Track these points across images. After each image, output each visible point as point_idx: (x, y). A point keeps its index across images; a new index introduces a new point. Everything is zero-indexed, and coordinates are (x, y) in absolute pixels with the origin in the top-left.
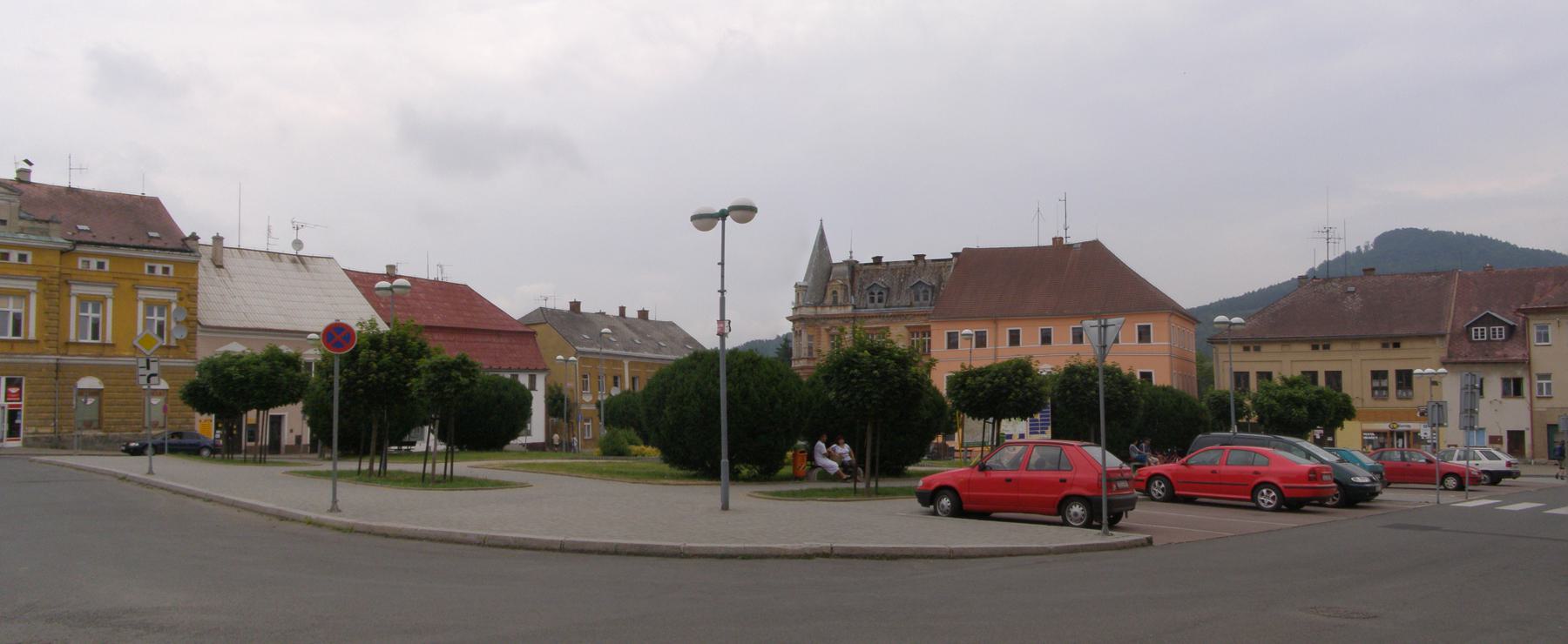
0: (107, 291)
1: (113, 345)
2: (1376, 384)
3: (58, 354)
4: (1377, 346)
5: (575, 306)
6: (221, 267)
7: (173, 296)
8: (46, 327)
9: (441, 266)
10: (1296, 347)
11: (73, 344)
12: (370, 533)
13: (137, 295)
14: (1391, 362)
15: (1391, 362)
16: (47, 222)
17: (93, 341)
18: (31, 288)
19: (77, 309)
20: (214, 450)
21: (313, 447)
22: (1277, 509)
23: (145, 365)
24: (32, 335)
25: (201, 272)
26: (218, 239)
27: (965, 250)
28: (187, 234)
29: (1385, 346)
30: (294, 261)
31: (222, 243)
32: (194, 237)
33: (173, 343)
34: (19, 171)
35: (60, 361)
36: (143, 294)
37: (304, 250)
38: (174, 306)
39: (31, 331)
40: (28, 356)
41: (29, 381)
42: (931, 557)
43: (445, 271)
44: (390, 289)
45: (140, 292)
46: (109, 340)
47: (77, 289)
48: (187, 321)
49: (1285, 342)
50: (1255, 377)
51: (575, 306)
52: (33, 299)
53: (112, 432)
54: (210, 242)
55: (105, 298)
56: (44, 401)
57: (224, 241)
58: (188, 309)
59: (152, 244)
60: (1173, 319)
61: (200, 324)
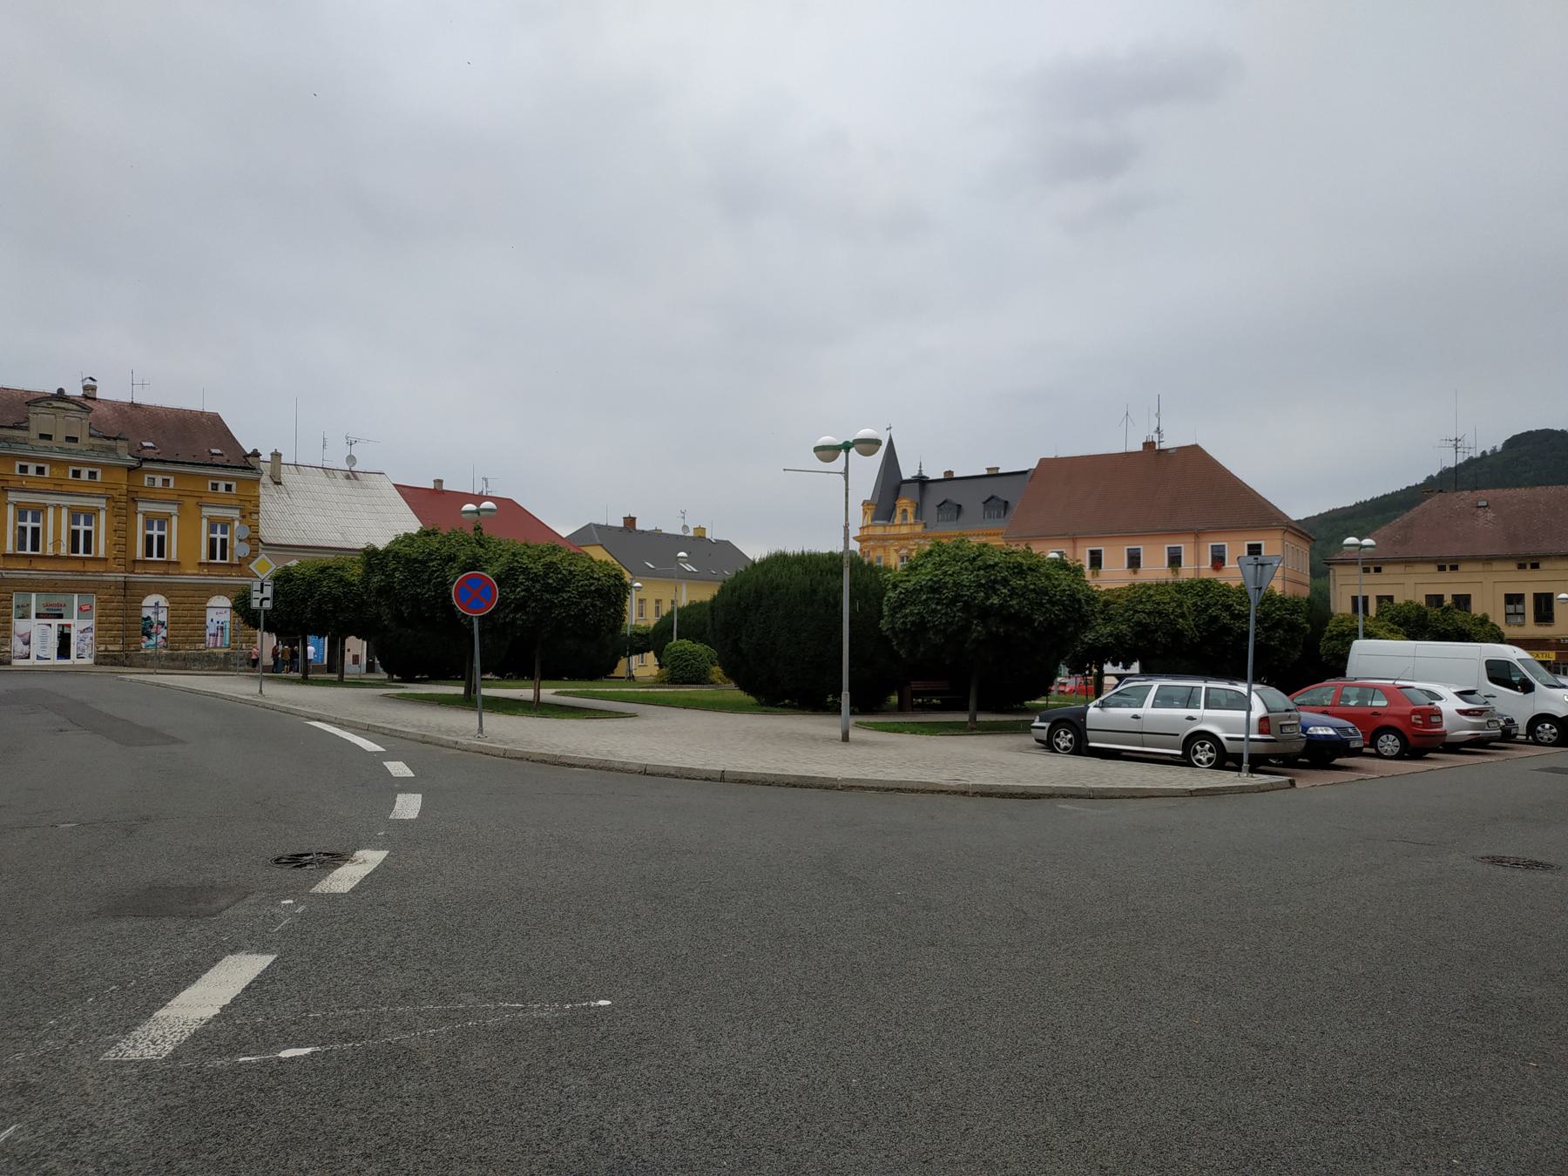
0: (173, 509)
1: (177, 563)
2: (1511, 608)
3: (126, 572)
4: (1513, 566)
5: (630, 521)
6: (280, 484)
7: (236, 514)
8: (115, 544)
9: (486, 480)
10: (1420, 568)
11: (139, 561)
12: (527, 759)
13: (201, 512)
14: (1529, 584)
15: (1529, 584)
16: (115, 439)
17: (33, 553)
18: (100, 506)
19: (15, 519)
20: (266, 669)
21: (276, 667)
22: (1399, 757)
23: (259, 589)
24: (102, 554)
25: (261, 490)
26: (276, 455)
27: (1043, 462)
28: (249, 451)
29: (1522, 567)
30: (348, 477)
31: (280, 460)
32: (256, 454)
33: (236, 561)
34: (85, 388)
35: (127, 579)
36: (207, 511)
37: (357, 465)
38: (237, 524)
39: (101, 548)
40: (97, 574)
41: (99, 599)
42: (1071, 796)
43: (489, 485)
44: (478, 512)
45: (204, 509)
46: (174, 557)
47: (142, 507)
48: (249, 539)
49: (1408, 562)
50: (1375, 602)
51: (630, 521)
52: (102, 515)
53: (176, 650)
54: (269, 458)
55: (171, 515)
56: (113, 619)
58: (250, 526)
59: (216, 460)
60: (1287, 536)
61: (262, 542)
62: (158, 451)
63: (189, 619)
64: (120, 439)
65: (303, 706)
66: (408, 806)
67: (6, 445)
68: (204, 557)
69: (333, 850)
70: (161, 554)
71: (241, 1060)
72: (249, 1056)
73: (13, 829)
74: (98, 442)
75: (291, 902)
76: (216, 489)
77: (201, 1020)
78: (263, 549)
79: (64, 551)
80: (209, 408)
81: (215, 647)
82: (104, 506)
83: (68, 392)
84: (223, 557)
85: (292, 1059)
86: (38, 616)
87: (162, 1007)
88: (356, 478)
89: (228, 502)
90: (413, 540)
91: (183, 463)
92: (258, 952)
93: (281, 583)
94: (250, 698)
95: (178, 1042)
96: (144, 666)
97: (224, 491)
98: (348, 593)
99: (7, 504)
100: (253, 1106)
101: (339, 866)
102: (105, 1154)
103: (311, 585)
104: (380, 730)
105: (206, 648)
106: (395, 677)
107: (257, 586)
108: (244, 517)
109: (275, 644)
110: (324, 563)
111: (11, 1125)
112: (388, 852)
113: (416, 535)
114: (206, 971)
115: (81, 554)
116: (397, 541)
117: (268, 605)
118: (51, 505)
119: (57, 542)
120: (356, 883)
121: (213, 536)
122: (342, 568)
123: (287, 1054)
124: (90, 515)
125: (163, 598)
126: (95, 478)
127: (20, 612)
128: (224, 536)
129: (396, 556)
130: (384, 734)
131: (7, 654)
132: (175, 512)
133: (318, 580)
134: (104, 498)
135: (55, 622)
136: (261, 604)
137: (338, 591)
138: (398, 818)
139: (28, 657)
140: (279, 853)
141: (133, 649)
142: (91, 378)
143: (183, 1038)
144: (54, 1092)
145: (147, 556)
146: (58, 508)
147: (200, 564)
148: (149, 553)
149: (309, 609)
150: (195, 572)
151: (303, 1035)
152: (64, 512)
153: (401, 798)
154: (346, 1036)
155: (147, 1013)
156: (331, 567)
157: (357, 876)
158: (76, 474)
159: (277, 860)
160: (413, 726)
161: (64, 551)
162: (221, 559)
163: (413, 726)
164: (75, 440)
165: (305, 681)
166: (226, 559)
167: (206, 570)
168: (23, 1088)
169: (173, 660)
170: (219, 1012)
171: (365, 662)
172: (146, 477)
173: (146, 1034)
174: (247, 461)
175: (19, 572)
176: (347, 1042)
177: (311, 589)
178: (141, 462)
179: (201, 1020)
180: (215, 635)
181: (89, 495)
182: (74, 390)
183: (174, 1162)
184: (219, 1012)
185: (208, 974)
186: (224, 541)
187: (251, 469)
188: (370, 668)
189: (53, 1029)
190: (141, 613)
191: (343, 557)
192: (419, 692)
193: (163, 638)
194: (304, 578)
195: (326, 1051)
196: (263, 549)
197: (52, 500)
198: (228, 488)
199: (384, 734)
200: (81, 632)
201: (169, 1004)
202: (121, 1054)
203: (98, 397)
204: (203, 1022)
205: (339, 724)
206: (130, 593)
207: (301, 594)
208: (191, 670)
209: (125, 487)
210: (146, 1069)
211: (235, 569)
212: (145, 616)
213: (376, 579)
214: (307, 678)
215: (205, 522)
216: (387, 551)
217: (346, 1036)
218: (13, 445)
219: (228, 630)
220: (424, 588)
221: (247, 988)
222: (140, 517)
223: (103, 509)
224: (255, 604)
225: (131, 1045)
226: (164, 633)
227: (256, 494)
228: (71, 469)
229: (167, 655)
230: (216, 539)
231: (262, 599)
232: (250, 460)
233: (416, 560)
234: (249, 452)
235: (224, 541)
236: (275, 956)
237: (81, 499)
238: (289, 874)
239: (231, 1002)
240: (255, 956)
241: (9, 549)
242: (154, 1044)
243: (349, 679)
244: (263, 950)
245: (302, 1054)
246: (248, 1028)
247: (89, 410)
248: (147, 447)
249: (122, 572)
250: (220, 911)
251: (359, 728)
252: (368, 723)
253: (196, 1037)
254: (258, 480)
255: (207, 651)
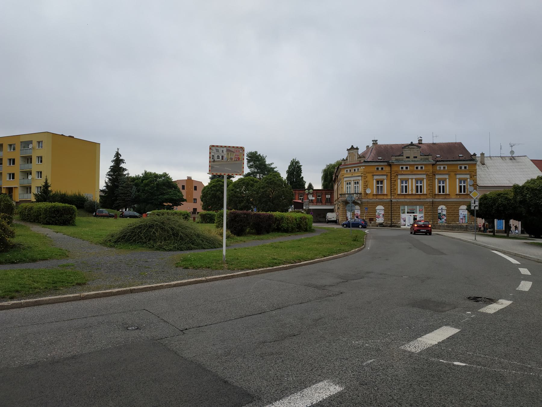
0: (447, 177)
1: (449, 195)
3: (433, 198)
6: (484, 164)
7: (468, 176)
8: (429, 189)
13: (456, 177)
16: (428, 155)
18: (424, 177)
24: (425, 193)
25: (477, 167)
26: (482, 154)
30: (511, 159)
31: (484, 156)
32: (475, 155)
34: (419, 141)
36: (458, 176)
38: (469, 180)
39: (425, 191)
45: (457, 176)
46: (448, 193)
47: (437, 177)
48: (473, 185)
53: (450, 224)
54: (480, 156)
55: (446, 179)
57: (485, 154)
58: (473, 180)
59: (461, 158)
61: (478, 186)
62: (442, 158)
63: (453, 214)
64: (429, 155)
65: (491, 245)
66: (525, 286)
67: (397, 161)
68: (458, 192)
69: (491, 298)
70: (443, 192)
71: (441, 361)
72: (443, 360)
73: (391, 276)
74: (423, 157)
75: (470, 313)
76: (461, 168)
77: (431, 344)
78: (478, 188)
79: (414, 192)
80: (458, 141)
81: (463, 223)
82: (425, 177)
83: (414, 143)
84: (464, 192)
85: (458, 366)
86: (408, 213)
87: (420, 337)
88: (514, 159)
89: (465, 172)
90: (535, 181)
91: (450, 161)
92: (454, 327)
93: (483, 200)
94: (471, 241)
95: (422, 349)
96: (439, 229)
97: (420, 169)
98: (509, 203)
99: (398, 179)
100: (441, 376)
101: (492, 304)
102: (394, 376)
103: (494, 200)
104: (520, 256)
105: (460, 223)
106: (532, 236)
107: (473, 202)
108: (471, 177)
109: (484, 222)
110: (499, 192)
111: (372, 359)
112: (512, 302)
113: (536, 180)
114: (436, 329)
115: (419, 193)
116: (528, 182)
117: (477, 208)
118: (410, 178)
119: (412, 190)
120: (496, 311)
121: (461, 185)
122: (507, 194)
123: (456, 363)
124: (421, 180)
125: (445, 206)
126: (445, 169)
127: (403, 211)
128: (464, 185)
129: (527, 188)
130: (521, 257)
131: (400, 224)
132: (448, 177)
133: (497, 198)
134: (425, 175)
135: (412, 215)
136: (475, 208)
137: (505, 202)
138: (519, 290)
139: (405, 225)
140: (470, 295)
141: (436, 223)
142: (421, 137)
143: (424, 348)
144: (385, 354)
145: (417, 193)
146: (412, 179)
147: (456, 194)
148: (440, 192)
149: (494, 209)
150: (455, 197)
151: (464, 359)
152: (414, 180)
153: (523, 282)
154: (479, 364)
155: (415, 338)
156: (502, 194)
157: (497, 308)
158: (417, 168)
159: (469, 298)
160: (534, 255)
161: (414, 192)
162: (464, 192)
163: (534, 255)
164: (416, 157)
165: (494, 236)
166: (444, 193)
167: (458, 197)
168: (378, 350)
169: (449, 227)
170: (437, 343)
171: (520, 230)
172: (438, 166)
173: (414, 344)
174: (472, 157)
175: (402, 199)
176: (479, 365)
177: (494, 202)
178: (436, 162)
179: (431, 344)
180: (462, 219)
181: (421, 174)
182: (416, 142)
183: (413, 385)
184: (437, 343)
185: (437, 330)
186: (464, 186)
187: (473, 160)
188: (522, 232)
189: (389, 335)
190: (438, 212)
191: (507, 189)
192: (539, 242)
193: (445, 220)
194: (491, 198)
195: (470, 366)
196: (478, 188)
197: (410, 177)
198: (465, 168)
199: (521, 257)
200: (420, 218)
201: (422, 337)
202: (405, 348)
203: (423, 143)
204: (431, 345)
205: (504, 252)
206: (434, 205)
207: (490, 204)
208: (455, 231)
209: (431, 171)
210: (411, 355)
211: (447, 196)
212: (439, 213)
213: (519, 198)
214: (495, 235)
215: (458, 180)
216: (523, 187)
217: (479, 364)
218: (399, 161)
219: (467, 217)
220: (540, 200)
221: (448, 338)
222: (436, 180)
223: (425, 178)
224: (472, 208)
225: (409, 346)
226: (445, 218)
227: (475, 169)
228: (415, 166)
229: (446, 225)
230: (441, 186)
231: (475, 206)
232: (473, 157)
233: (536, 189)
234: (472, 154)
235: (464, 186)
236: (460, 330)
237: (420, 176)
238: (472, 303)
239: (442, 341)
240: (453, 328)
241: (399, 192)
242: (415, 348)
243: (511, 236)
244: (456, 327)
245: (462, 365)
246: (445, 351)
247: (420, 147)
248: (438, 157)
249: (432, 198)
250: (445, 311)
251: (512, 255)
252: (515, 252)
253: (428, 349)
254: (476, 164)
255: (460, 224)
